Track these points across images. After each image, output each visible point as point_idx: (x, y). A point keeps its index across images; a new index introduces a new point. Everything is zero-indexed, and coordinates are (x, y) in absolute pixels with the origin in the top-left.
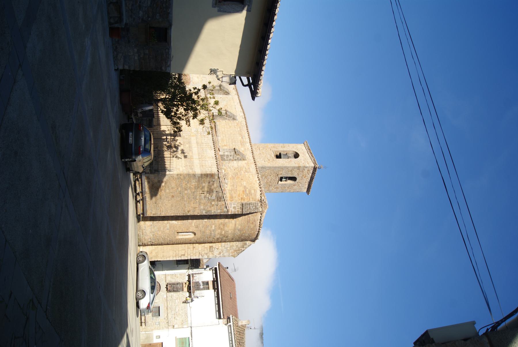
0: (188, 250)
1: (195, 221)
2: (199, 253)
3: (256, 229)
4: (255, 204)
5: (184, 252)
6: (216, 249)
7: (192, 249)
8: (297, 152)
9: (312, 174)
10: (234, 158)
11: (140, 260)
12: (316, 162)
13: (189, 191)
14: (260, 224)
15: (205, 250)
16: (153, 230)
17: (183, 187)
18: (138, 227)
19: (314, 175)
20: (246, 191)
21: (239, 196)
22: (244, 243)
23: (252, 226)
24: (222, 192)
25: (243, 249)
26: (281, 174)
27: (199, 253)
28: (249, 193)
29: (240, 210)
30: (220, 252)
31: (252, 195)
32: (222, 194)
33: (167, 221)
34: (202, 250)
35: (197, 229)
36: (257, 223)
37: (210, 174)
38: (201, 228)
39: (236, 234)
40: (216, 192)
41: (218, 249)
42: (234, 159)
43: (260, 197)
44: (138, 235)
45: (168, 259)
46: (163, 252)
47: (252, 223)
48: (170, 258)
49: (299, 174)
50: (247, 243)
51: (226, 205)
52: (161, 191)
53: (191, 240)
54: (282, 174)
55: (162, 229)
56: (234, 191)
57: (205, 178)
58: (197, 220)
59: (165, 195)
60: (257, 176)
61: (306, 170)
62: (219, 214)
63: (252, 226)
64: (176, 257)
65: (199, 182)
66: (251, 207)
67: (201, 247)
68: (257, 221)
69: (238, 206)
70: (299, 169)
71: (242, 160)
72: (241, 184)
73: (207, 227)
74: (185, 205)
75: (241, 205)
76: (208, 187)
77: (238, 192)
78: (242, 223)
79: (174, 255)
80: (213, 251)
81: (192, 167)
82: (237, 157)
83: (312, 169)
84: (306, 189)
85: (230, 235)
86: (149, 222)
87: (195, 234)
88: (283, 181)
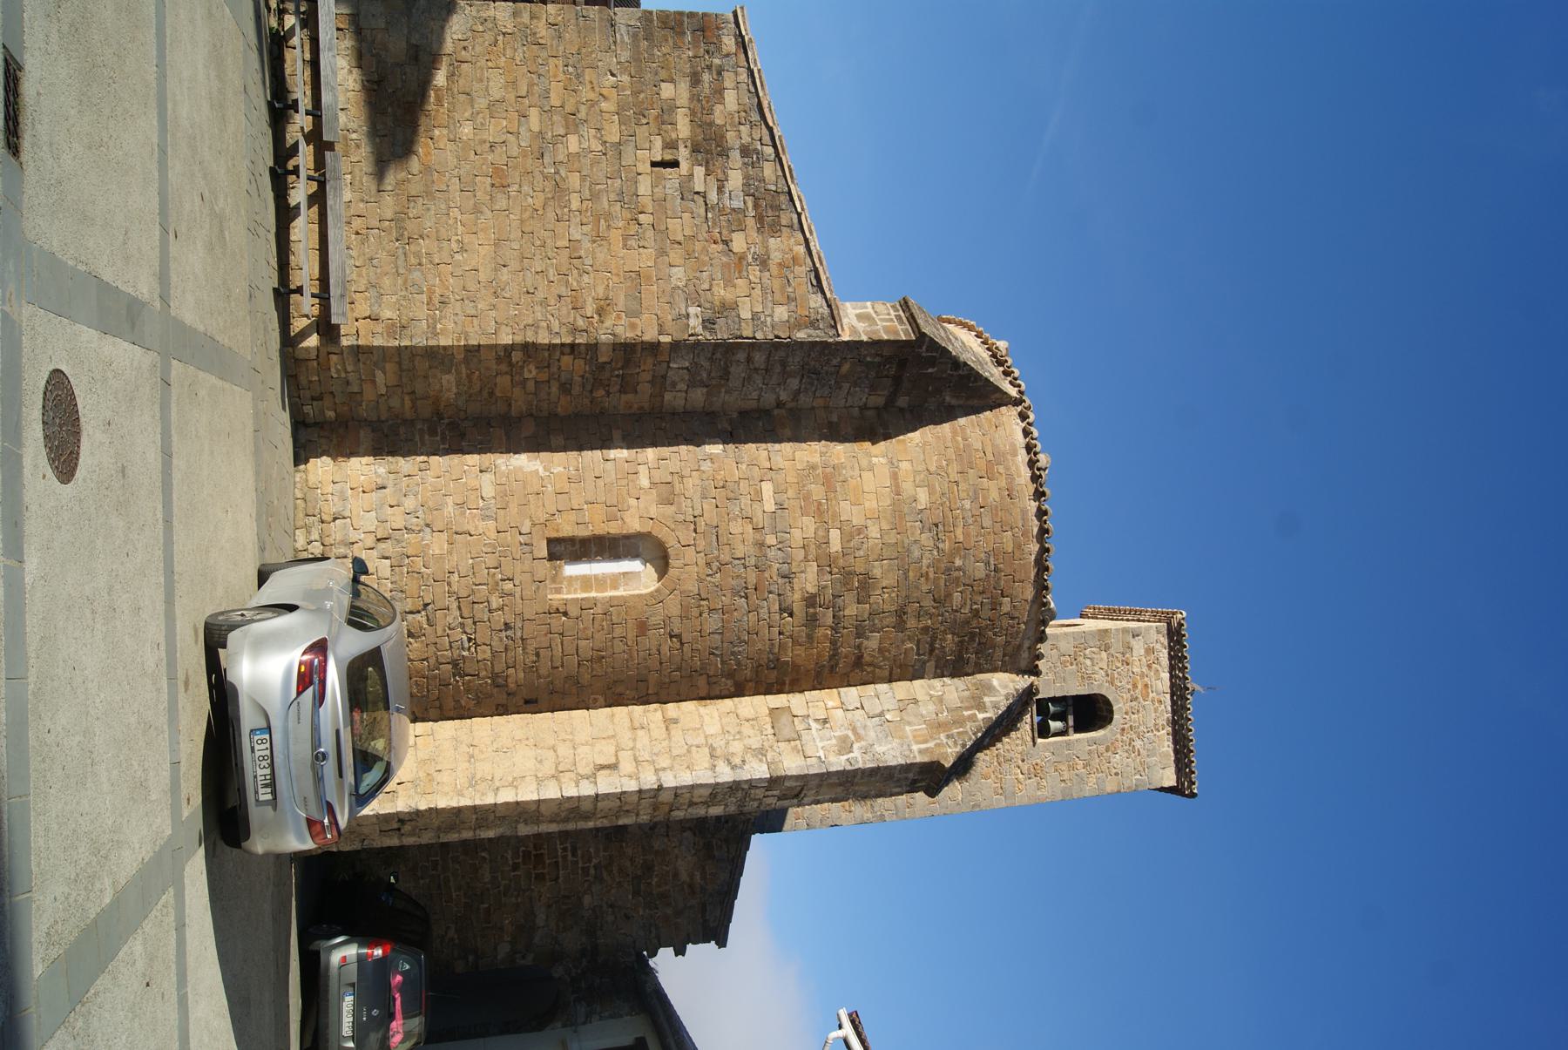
0: (634, 740)
1: (651, 453)
2: (712, 749)
3: (1024, 512)
5: (612, 749)
6: (817, 720)
9: (1172, 668)
14: (1035, 478)
24: (777, 154)
30: (844, 739)
32: (780, 173)
34: (725, 732)
35: (673, 508)
38: (698, 506)
39: (917, 554)
40: (745, 151)
41: (825, 721)
45: (507, 796)
48: (516, 787)
50: (995, 683)
51: (816, 260)
76: (693, 113)
78: (933, 469)
79: (548, 770)
80: (799, 738)
84: (1173, 769)
85: (877, 572)
86: (365, 460)
87: (661, 560)
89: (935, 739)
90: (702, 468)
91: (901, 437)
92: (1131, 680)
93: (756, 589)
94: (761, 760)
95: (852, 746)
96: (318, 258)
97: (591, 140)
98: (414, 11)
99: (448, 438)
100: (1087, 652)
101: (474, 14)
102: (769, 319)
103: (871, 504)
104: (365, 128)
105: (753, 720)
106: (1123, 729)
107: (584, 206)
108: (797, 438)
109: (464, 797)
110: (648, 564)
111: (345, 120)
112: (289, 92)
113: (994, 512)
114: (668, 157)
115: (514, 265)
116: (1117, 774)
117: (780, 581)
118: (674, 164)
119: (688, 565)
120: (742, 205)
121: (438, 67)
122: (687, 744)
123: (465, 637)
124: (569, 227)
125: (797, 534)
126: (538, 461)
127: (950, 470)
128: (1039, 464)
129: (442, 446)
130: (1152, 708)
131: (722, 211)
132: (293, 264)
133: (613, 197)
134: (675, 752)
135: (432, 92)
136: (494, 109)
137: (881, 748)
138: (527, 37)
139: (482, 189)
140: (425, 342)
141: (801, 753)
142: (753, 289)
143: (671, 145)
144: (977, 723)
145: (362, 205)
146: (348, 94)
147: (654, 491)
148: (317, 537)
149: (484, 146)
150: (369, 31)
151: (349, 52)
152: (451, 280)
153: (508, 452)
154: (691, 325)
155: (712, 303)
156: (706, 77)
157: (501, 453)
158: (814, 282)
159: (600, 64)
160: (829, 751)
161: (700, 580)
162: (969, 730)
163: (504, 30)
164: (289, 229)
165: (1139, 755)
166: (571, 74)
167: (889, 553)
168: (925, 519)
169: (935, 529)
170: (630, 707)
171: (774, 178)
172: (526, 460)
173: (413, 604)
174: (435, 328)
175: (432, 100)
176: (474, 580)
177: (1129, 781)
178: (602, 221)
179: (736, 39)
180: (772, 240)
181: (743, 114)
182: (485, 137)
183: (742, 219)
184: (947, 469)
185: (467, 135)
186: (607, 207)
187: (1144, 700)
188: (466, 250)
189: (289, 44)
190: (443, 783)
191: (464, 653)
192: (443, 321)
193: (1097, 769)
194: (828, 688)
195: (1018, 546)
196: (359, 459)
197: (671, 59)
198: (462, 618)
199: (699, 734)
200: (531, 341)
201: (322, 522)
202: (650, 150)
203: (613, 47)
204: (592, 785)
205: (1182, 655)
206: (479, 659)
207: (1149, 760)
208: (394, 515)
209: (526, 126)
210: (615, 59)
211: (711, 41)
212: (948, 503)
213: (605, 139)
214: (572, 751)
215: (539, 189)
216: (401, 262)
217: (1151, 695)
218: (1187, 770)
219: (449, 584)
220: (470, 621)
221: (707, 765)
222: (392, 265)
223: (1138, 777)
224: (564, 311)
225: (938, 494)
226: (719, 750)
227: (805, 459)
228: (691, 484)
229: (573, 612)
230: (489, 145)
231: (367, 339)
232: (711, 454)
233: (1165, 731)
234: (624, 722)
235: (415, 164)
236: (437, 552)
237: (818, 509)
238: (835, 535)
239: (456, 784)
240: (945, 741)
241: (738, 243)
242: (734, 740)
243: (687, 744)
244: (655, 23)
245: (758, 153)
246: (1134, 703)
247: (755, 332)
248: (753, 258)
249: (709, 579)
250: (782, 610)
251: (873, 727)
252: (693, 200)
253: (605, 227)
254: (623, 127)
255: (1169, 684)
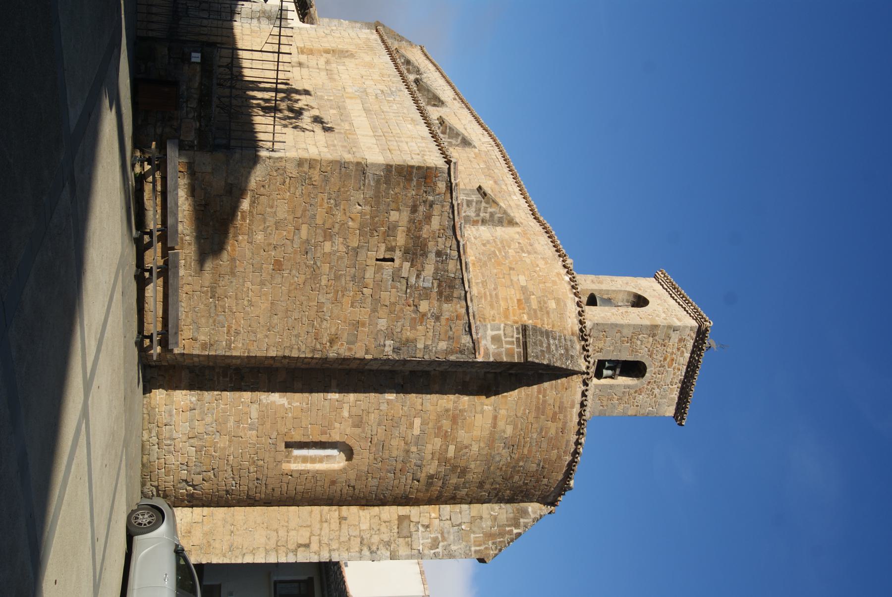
0: (321, 529)
1: (352, 397)
2: (362, 539)
3: (568, 441)
4: (563, 340)
5: (308, 534)
6: (423, 526)
7: (335, 525)
8: (640, 293)
9: (693, 352)
10: (478, 215)
11: (140, 524)
12: (702, 313)
13: (338, 245)
14: (580, 424)
15: (383, 528)
16: (200, 427)
17: (319, 221)
18: (145, 411)
19: (699, 356)
20: (527, 300)
21: (507, 317)
22: (518, 510)
23: (552, 429)
24: (459, 256)
25: (515, 531)
26: (601, 350)
27: (362, 539)
28: (541, 309)
29: (517, 350)
31: (552, 315)
32: (459, 267)
33: (249, 393)
34: (371, 529)
35: (360, 430)
36: (572, 415)
37: (419, 168)
39: (498, 459)
40: (439, 254)
41: (427, 527)
42: (479, 218)
43: (576, 321)
44: (143, 446)
45: (248, 560)
46: (232, 532)
47: (554, 419)
48: (254, 554)
49: (652, 353)
50: (530, 510)
51: (471, 318)
52: (235, 236)
53: (333, 483)
54: (604, 351)
55: (231, 424)
56: (489, 298)
57: (402, 185)
58: (360, 392)
59: (248, 254)
60: (560, 263)
61: (675, 337)
62: (442, 358)
63: (552, 429)
64: (277, 551)
65: (378, 203)
66: (553, 347)
67: (368, 517)
68: (569, 409)
69: (511, 334)
70: (654, 335)
71: (505, 222)
72: (512, 280)
73: (394, 423)
74: (320, 305)
75: (518, 333)
76: (409, 230)
77: (502, 303)
78: (519, 415)
79: (272, 544)
80: (411, 536)
81: (354, 149)
82: (490, 210)
83: (691, 337)
84: (674, 407)
85: (472, 466)
86: (184, 392)
87: (349, 453)
88: (606, 378)
89: (486, 544)
90: (381, 408)
91: (505, 394)
92: (663, 355)
93: (400, 471)
94: (387, 549)
95: (438, 545)
96: (162, 307)
97: (340, 245)
98: (231, 161)
99: (234, 379)
100: (640, 336)
101: (272, 164)
102: (434, 349)
103: (476, 433)
104: (194, 234)
105: (388, 522)
106: (649, 382)
107: (330, 284)
108: (442, 392)
109: (226, 557)
110: (341, 452)
111: (182, 229)
112: (147, 210)
113: (550, 440)
114: (387, 256)
115: (280, 315)
116: (637, 406)
117: (415, 468)
118: (392, 260)
119: (363, 458)
120: (430, 285)
121: (245, 198)
122: (349, 535)
123: (234, 482)
124: (319, 295)
125: (429, 447)
126: (285, 398)
127: (530, 416)
128: (584, 417)
129: (230, 385)
130: (673, 372)
131: (417, 288)
132: (146, 309)
133: (348, 278)
134: (342, 539)
135: (239, 213)
136: (279, 224)
137: (455, 547)
138: (305, 180)
139: (267, 272)
140: (224, 353)
141: (410, 546)
142: (428, 332)
143: (391, 249)
144: (512, 536)
145: (190, 278)
146: (185, 212)
147: (350, 420)
148: (155, 434)
149: (270, 247)
150: (200, 174)
151: (186, 186)
152: (242, 322)
153: (268, 391)
154: (386, 350)
155: (401, 339)
156: (422, 209)
157: (264, 392)
158: (467, 329)
159: (352, 198)
160: (425, 547)
161: (369, 465)
162: (506, 540)
163: (290, 175)
164: (144, 289)
165: (655, 397)
166: (331, 204)
167: (481, 458)
168: (507, 442)
169: (512, 447)
170: (322, 507)
171: (454, 270)
172: (278, 397)
173: (207, 468)
174: (230, 346)
175: (239, 218)
176: (242, 459)
177: (644, 411)
178: (340, 292)
179: (447, 184)
180: (445, 306)
181: (442, 231)
182: (271, 242)
183: (429, 294)
184: (528, 416)
185: (259, 240)
186: (344, 284)
187: (669, 368)
188: (253, 306)
189: (147, 180)
190: (216, 548)
191: (233, 488)
192: (236, 343)
193: (626, 402)
194: (434, 505)
195: (559, 457)
196: (181, 391)
197: (400, 196)
198: (233, 475)
199: (356, 529)
200: (287, 355)
201: (158, 427)
202: (377, 252)
203: (362, 188)
204: (294, 556)
205: (702, 347)
206: (241, 490)
207: (660, 400)
208: (199, 425)
209: (299, 236)
210: (362, 196)
211: (428, 185)
212: (523, 434)
213: (349, 244)
214: (286, 534)
215: (302, 273)
216: (212, 310)
217: (674, 365)
218: (683, 411)
219: (228, 460)
220: (237, 476)
221: (357, 549)
222: (207, 312)
223: (651, 409)
224: (309, 340)
225: (519, 429)
226: (365, 540)
227: (444, 405)
228: (373, 417)
229: (295, 475)
230: (273, 246)
231: (189, 350)
232: (388, 399)
233: (676, 386)
234: (317, 517)
235: (225, 255)
236: (222, 445)
237: (445, 434)
238: (452, 448)
239: (222, 549)
240: (491, 545)
241: (424, 306)
242: (375, 534)
243: (349, 535)
244: (393, 173)
245: (447, 255)
246: (662, 369)
247: (424, 355)
248: (431, 315)
249: (375, 465)
250: (413, 479)
251: (453, 533)
252: (400, 282)
253: (341, 295)
254: (361, 238)
255: (688, 360)
